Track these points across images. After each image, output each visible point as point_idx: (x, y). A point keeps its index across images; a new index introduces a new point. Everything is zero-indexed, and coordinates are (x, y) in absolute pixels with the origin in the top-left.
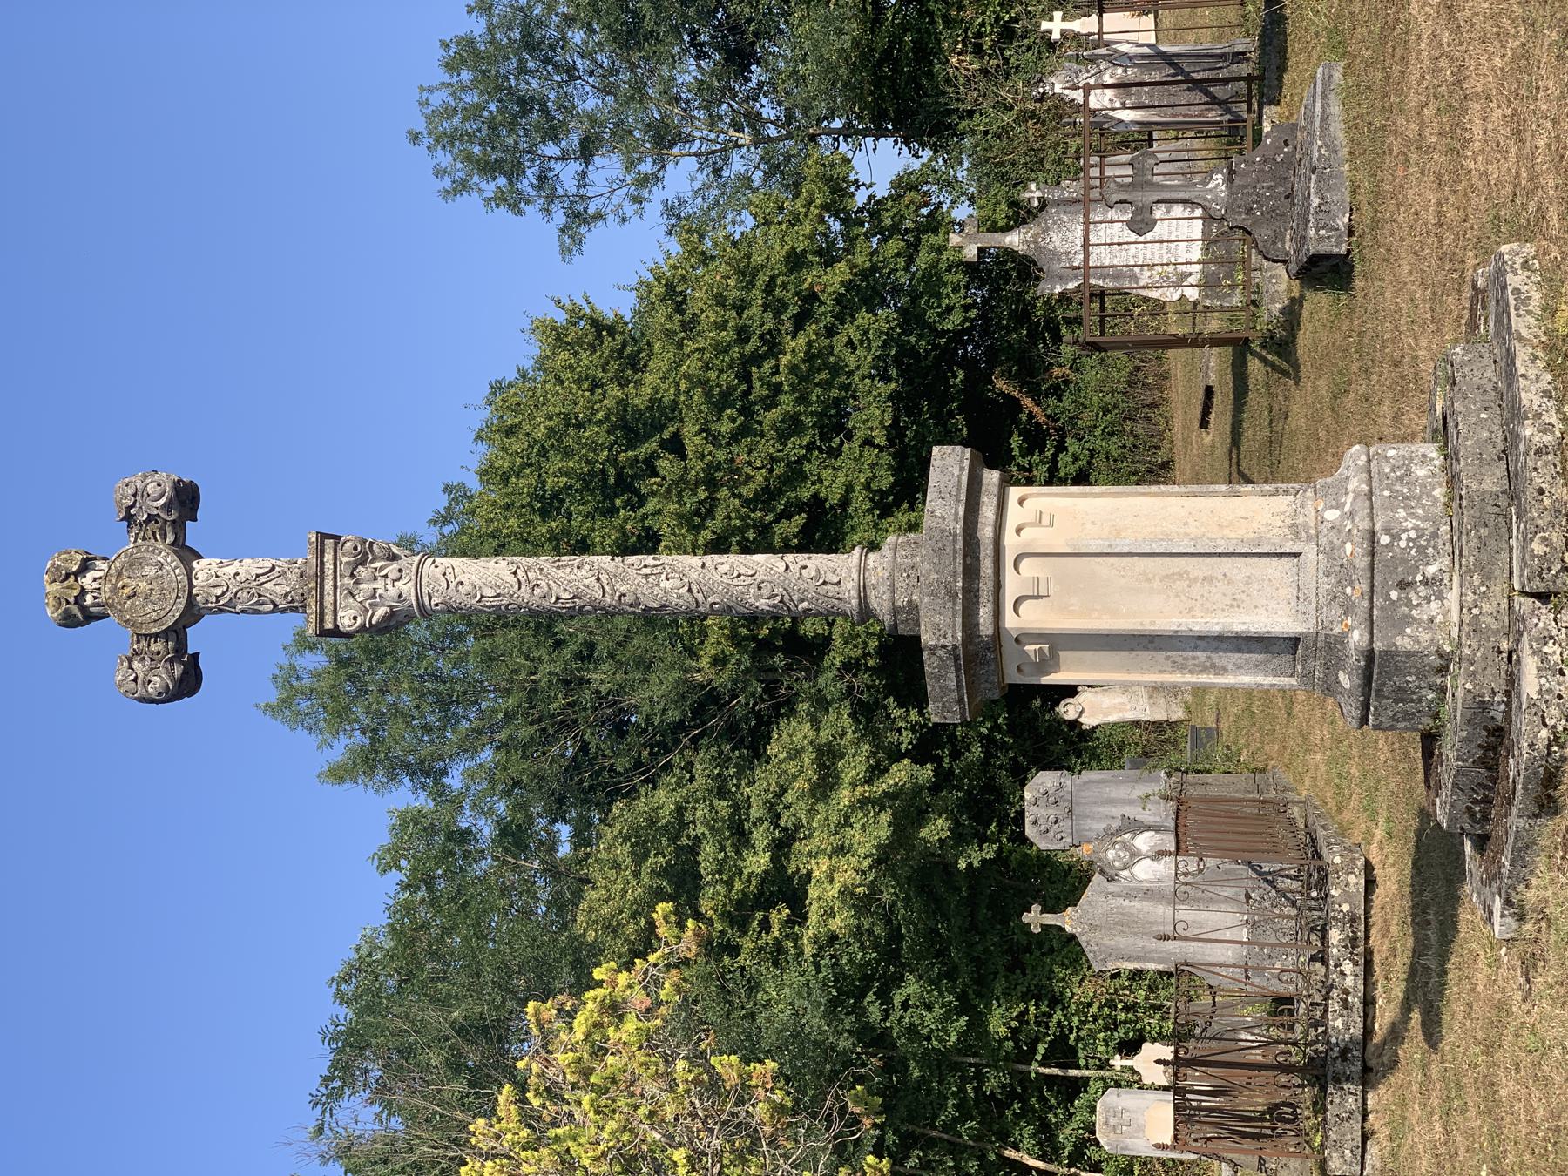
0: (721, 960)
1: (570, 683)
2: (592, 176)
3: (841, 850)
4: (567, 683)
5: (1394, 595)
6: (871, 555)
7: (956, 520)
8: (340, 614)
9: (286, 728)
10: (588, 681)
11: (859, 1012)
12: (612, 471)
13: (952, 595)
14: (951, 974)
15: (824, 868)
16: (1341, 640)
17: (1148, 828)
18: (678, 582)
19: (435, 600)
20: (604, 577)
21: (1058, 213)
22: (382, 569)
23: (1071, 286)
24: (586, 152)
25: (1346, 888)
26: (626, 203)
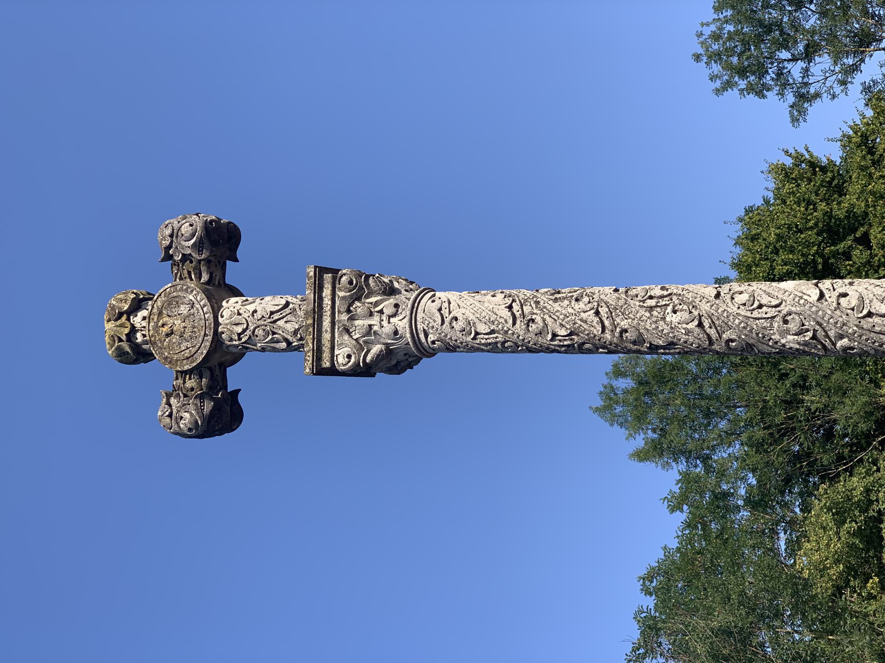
1: (792, 403)
8: (337, 352)
9: (607, 424)
10: (803, 401)
12: (820, 260)
18: (685, 316)
19: (431, 337)
20: (603, 311)
22: (376, 304)
24: (809, 54)
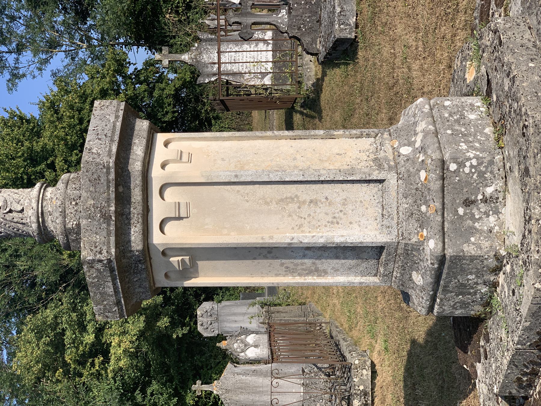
0: (75, 379)
2: (21, 58)
3: (124, 333)
4: (8, 267)
5: (461, 211)
6: (50, 190)
7: (110, 155)
11: (133, 398)
13: (106, 218)
14: (171, 380)
15: (117, 341)
16: (418, 248)
17: (253, 332)
21: (206, 45)
23: (213, 79)
24: (19, 49)
25: (361, 378)
26: (35, 70)
